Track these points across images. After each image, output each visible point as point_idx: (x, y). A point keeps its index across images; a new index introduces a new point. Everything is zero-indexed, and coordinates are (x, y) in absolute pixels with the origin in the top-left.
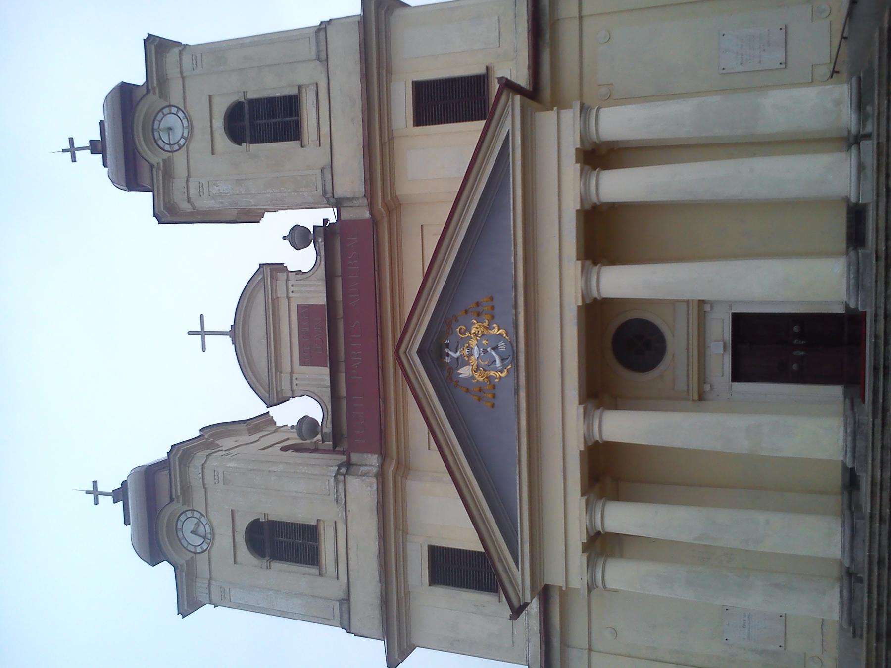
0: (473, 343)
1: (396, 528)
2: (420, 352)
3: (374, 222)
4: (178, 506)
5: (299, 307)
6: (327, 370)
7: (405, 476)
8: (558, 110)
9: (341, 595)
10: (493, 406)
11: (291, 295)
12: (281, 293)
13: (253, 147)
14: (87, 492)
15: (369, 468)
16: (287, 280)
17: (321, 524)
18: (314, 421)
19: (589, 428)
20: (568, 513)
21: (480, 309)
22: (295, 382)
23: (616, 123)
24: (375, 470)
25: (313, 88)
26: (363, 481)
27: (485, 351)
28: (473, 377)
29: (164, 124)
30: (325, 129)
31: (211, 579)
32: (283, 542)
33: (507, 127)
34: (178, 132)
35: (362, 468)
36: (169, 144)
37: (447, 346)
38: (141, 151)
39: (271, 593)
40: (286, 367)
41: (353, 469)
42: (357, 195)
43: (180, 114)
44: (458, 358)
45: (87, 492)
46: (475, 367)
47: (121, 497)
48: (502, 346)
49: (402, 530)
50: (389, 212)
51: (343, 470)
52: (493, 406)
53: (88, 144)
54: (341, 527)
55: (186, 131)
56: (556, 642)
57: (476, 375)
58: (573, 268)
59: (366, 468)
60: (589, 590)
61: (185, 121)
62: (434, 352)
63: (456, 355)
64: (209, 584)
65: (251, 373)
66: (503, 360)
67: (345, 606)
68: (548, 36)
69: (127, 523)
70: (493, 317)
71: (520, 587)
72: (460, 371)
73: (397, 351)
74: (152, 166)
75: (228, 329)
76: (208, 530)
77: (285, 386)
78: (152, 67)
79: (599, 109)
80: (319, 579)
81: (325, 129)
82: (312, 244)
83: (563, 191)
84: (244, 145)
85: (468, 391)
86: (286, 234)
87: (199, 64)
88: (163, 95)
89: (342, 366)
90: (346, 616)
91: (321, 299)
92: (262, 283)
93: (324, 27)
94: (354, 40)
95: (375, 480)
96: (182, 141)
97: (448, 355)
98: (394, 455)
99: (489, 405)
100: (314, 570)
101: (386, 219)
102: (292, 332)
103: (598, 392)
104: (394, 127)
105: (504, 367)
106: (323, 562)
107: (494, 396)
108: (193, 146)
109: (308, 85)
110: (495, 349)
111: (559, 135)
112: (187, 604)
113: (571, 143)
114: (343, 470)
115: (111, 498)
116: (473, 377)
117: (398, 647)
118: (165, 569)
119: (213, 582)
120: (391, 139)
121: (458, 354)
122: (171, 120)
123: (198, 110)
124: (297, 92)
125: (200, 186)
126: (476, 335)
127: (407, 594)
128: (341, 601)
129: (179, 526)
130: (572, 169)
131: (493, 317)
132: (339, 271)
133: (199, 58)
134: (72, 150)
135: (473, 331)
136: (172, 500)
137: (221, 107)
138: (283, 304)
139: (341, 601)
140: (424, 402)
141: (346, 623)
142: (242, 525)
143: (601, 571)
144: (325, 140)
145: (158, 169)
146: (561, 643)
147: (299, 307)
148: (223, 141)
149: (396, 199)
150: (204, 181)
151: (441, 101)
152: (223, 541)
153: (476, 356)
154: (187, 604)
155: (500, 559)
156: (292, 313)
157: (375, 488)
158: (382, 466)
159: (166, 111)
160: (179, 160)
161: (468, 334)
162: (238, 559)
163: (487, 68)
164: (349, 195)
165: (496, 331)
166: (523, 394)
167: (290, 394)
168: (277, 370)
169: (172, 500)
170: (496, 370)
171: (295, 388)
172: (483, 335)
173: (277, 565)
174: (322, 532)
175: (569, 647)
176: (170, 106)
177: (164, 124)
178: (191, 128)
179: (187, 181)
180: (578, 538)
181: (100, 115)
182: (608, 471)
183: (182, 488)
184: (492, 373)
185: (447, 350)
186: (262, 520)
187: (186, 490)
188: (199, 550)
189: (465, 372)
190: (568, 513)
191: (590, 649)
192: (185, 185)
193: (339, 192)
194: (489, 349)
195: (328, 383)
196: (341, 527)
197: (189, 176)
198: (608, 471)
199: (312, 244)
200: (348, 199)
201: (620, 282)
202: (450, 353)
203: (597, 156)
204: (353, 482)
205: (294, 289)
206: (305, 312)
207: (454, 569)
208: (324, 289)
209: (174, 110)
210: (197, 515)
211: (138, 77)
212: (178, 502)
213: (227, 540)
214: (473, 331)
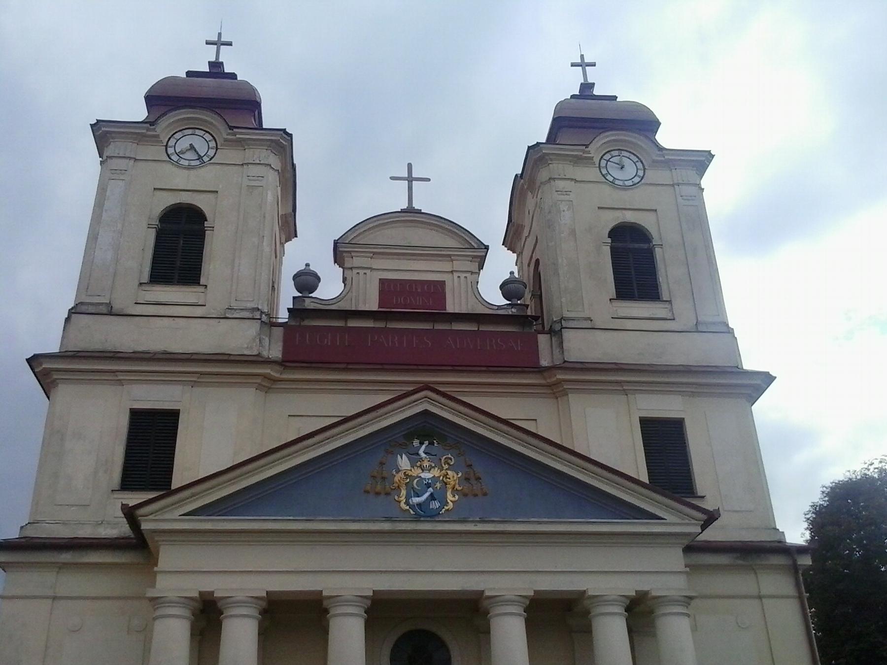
0: (436, 472)
1: (202, 374)
2: (426, 412)
3: (540, 370)
4: (223, 133)
5: (443, 283)
6: (373, 306)
7: (260, 387)
8: (686, 573)
9: (117, 306)
10: (367, 492)
11: (456, 275)
12: (458, 265)
13: (607, 250)
14: (220, 35)
15: (267, 348)
16: (472, 273)
17: (202, 289)
18: (313, 288)
19: (347, 602)
20: (247, 573)
21: (473, 482)
22: (362, 272)
23: (675, 630)
24: (265, 354)
25: (669, 316)
26: (254, 340)
27: (428, 486)
28: (398, 471)
29: (626, 161)
30: (629, 324)
31: (136, 160)
32: (179, 246)
33: (669, 517)
34: (615, 173)
35: (267, 339)
36: (608, 161)
37: (431, 443)
38: (602, 136)
39: (119, 226)
40: (378, 263)
41: (266, 328)
42: (565, 353)
43: (637, 180)
44: (418, 454)
45: (220, 35)
46: (410, 473)
47: (215, 71)
48: (435, 505)
49: (198, 381)
50: (549, 386)
51: (264, 318)
52: (367, 492)
53: (590, 81)
54: (199, 311)
55: (621, 183)
56: (66, 557)
57: (401, 474)
58: (527, 586)
59: (267, 344)
60: (153, 599)
61: (630, 183)
62: (426, 429)
63: (421, 452)
64: (130, 158)
65: (371, 225)
66: (419, 505)
67: (104, 309)
68: (740, 562)
69: (190, 74)
70: (465, 495)
71: (161, 517)
72: (404, 456)
73: (427, 387)
74: (587, 146)
75: (416, 205)
76: (182, 162)
77: (357, 261)
78: (114, 127)
79: (688, 615)
80: (138, 283)
81: (629, 324)
82: (508, 302)
83: (604, 574)
84: (609, 240)
85: (382, 464)
86: (311, 268)
87: (687, 203)
88: (656, 164)
89: (380, 325)
90: (91, 309)
91: (452, 307)
92: (467, 246)
93: (730, 331)
94: (718, 360)
95: (255, 353)
96: (611, 179)
97: (422, 443)
98: (285, 376)
99: (368, 488)
100: (146, 278)
101: (543, 382)
102: (416, 273)
103: (380, 611)
104: (639, 396)
105: (412, 507)
106: (154, 288)
107: (378, 494)
108: (607, 189)
109: (671, 310)
110: (432, 497)
111: (659, 571)
112: (104, 133)
113: (654, 586)
114: (264, 318)
115: (213, 59)
116: (398, 471)
117: (45, 370)
118: (139, 112)
119: (132, 162)
120: (626, 393)
121: (423, 455)
122: (630, 170)
123: (205, 177)
124: (201, 283)
125: (567, 193)
126: (446, 476)
127: (120, 382)
128: (109, 305)
129: (197, 132)
130: (629, 587)
131: (465, 495)
132: (483, 328)
133: (691, 203)
134: (219, 43)
135: (449, 472)
136: (231, 128)
137: (646, 221)
138: (447, 266)
139: (109, 305)
140: (373, 414)
141: (83, 308)
142: (199, 201)
143: (178, 613)
144: (617, 324)
145: (148, 130)
146: (64, 564)
147: (443, 283)
148: (611, 220)
149: (565, 393)
150: (572, 196)
151: (665, 443)
152: (179, 179)
153: (423, 475)
154: (104, 133)
155: (193, 495)
156: (403, 273)
157: (246, 352)
158: (268, 362)
159: (212, 144)
160: (591, 173)
161: (446, 466)
162: (158, 193)
163: (703, 497)
164: (565, 345)
165: (450, 497)
166: (387, 526)
167: (346, 265)
168: (374, 253)
169: (231, 128)
170: (408, 497)
171: (355, 271)
172: (446, 484)
173: (152, 235)
174: (195, 290)
175: (58, 572)
176: (645, 169)
177: (626, 161)
178: (625, 188)
179: (572, 180)
180: (218, 586)
181: (623, 97)
182: (208, 616)
183: (244, 140)
184: (404, 492)
185: (427, 443)
186: (206, 224)
187: (241, 144)
188: (171, 151)
189: (404, 462)
190: (247, 573)
191: (55, 598)
192: (127, 155)
193: (567, 335)
194: (431, 489)
195: (362, 308)
196: (199, 311)
197: (576, 181)
198: (208, 616)
199: (508, 302)
200: (561, 343)
201: (510, 635)
202: (424, 447)
203: (640, 613)
204: (251, 329)
205: (462, 278)
206: (437, 290)
207: (150, 445)
208: (464, 311)
209: (641, 173)
210: (211, 153)
211: (665, 138)
212: (228, 134)
213: (181, 183)
214: (449, 472)
